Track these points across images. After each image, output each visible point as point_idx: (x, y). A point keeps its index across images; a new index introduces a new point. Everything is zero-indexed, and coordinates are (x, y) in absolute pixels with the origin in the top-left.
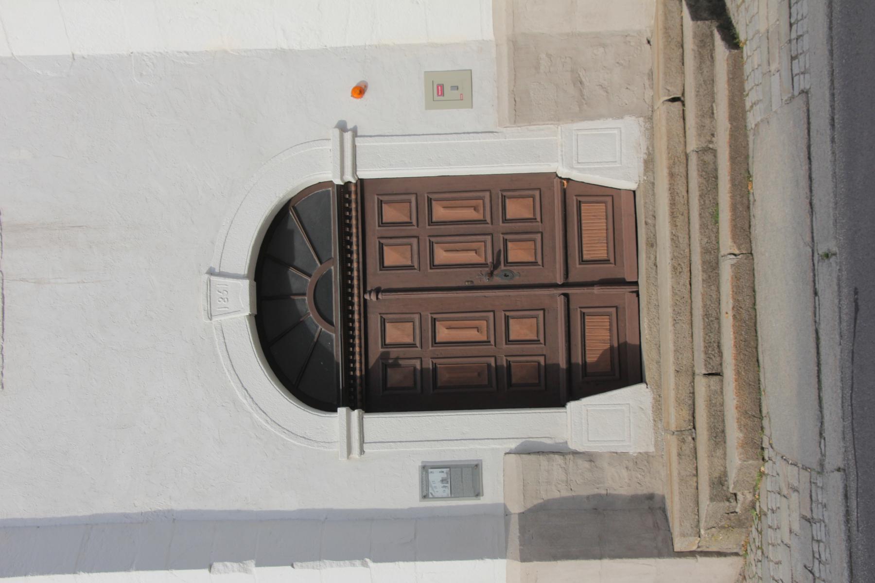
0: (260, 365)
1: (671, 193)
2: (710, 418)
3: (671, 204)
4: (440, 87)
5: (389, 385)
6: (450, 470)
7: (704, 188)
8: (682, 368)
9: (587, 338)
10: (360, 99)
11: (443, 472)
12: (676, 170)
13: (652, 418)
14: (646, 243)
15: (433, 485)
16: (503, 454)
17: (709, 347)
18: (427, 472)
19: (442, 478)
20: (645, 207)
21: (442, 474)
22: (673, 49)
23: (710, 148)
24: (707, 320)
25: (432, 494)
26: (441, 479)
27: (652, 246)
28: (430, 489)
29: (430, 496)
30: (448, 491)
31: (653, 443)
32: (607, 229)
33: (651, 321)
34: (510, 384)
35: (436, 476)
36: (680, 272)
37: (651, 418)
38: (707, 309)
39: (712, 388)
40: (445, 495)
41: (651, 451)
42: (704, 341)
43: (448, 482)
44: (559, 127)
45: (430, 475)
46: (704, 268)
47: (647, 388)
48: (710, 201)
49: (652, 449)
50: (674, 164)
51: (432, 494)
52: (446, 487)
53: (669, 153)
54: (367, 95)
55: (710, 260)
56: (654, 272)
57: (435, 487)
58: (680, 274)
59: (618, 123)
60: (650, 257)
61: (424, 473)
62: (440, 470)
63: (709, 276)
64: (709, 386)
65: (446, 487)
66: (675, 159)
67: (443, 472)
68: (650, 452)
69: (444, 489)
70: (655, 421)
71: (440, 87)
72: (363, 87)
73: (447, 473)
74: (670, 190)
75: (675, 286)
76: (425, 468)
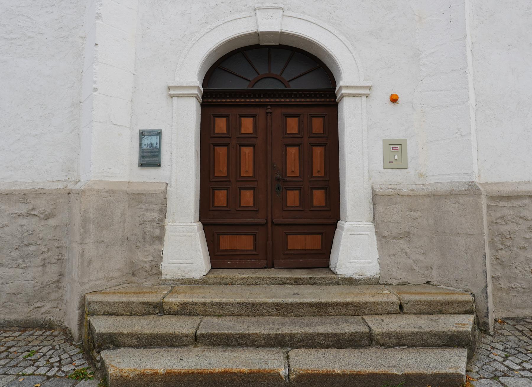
0: (231, 36)
1: (334, 304)
2: (161, 336)
3: (326, 303)
4: (397, 149)
5: (217, 119)
6: (158, 149)
7: (342, 337)
8: (208, 307)
9: (237, 236)
10: (389, 99)
11: (157, 144)
12: (351, 308)
13: (183, 278)
14: (297, 278)
15: (149, 138)
16: (167, 182)
17: (217, 338)
18: (157, 135)
19: (153, 144)
20: (321, 277)
21: (156, 144)
22: (437, 307)
23: (372, 341)
24: (237, 337)
25: (143, 137)
26: (153, 143)
27: (296, 282)
28: (147, 136)
29: (142, 137)
30: (145, 147)
31: (168, 278)
32: (305, 250)
33: (246, 280)
34: (214, 189)
35: (154, 140)
36: (276, 309)
37: (183, 278)
38: (246, 337)
39: (185, 338)
40: (143, 145)
41: (162, 277)
42: (221, 334)
43: (151, 147)
44: (372, 223)
45: (155, 136)
46: (278, 336)
47: (203, 275)
48: (331, 342)
49: (164, 277)
50: (355, 307)
51: (143, 137)
52: (148, 146)
53: (362, 303)
54: (392, 104)
55: (285, 341)
56: (278, 282)
57: (148, 139)
58: (275, 309)
59: (376, 262)
60: (288, 280)
61: (157, 133)
62: (158, 143)
63: (272, 340)
64: (186, 336)
65: (148, 146)
66: (358, 307)
67: (157, 144)
68: (161, 276)
69: (146, 145)
70: (182, 279)
71: (397, 149)
72: (397, 102)
73: (156, 147)
74: (336, 303)
75: (266, 305)
76: (159, 134)
